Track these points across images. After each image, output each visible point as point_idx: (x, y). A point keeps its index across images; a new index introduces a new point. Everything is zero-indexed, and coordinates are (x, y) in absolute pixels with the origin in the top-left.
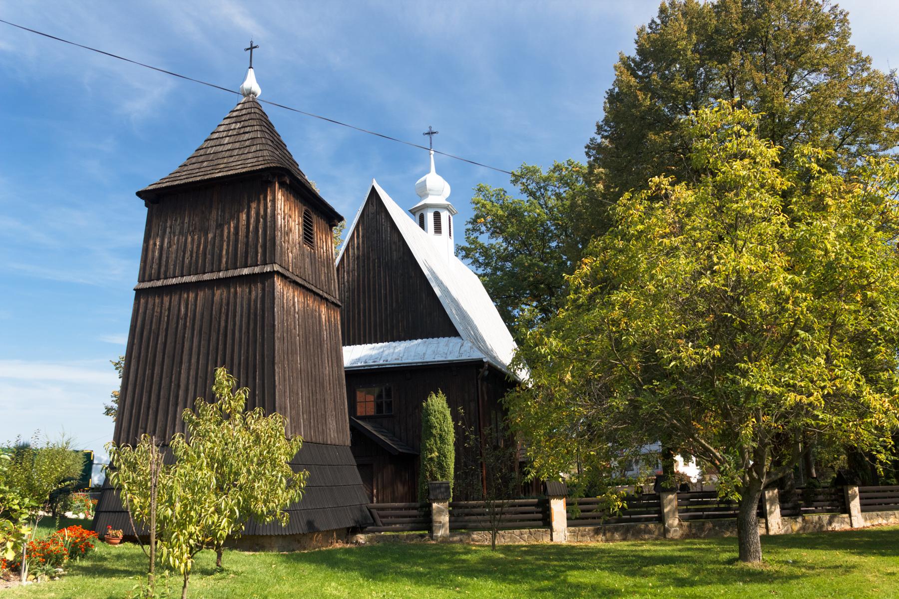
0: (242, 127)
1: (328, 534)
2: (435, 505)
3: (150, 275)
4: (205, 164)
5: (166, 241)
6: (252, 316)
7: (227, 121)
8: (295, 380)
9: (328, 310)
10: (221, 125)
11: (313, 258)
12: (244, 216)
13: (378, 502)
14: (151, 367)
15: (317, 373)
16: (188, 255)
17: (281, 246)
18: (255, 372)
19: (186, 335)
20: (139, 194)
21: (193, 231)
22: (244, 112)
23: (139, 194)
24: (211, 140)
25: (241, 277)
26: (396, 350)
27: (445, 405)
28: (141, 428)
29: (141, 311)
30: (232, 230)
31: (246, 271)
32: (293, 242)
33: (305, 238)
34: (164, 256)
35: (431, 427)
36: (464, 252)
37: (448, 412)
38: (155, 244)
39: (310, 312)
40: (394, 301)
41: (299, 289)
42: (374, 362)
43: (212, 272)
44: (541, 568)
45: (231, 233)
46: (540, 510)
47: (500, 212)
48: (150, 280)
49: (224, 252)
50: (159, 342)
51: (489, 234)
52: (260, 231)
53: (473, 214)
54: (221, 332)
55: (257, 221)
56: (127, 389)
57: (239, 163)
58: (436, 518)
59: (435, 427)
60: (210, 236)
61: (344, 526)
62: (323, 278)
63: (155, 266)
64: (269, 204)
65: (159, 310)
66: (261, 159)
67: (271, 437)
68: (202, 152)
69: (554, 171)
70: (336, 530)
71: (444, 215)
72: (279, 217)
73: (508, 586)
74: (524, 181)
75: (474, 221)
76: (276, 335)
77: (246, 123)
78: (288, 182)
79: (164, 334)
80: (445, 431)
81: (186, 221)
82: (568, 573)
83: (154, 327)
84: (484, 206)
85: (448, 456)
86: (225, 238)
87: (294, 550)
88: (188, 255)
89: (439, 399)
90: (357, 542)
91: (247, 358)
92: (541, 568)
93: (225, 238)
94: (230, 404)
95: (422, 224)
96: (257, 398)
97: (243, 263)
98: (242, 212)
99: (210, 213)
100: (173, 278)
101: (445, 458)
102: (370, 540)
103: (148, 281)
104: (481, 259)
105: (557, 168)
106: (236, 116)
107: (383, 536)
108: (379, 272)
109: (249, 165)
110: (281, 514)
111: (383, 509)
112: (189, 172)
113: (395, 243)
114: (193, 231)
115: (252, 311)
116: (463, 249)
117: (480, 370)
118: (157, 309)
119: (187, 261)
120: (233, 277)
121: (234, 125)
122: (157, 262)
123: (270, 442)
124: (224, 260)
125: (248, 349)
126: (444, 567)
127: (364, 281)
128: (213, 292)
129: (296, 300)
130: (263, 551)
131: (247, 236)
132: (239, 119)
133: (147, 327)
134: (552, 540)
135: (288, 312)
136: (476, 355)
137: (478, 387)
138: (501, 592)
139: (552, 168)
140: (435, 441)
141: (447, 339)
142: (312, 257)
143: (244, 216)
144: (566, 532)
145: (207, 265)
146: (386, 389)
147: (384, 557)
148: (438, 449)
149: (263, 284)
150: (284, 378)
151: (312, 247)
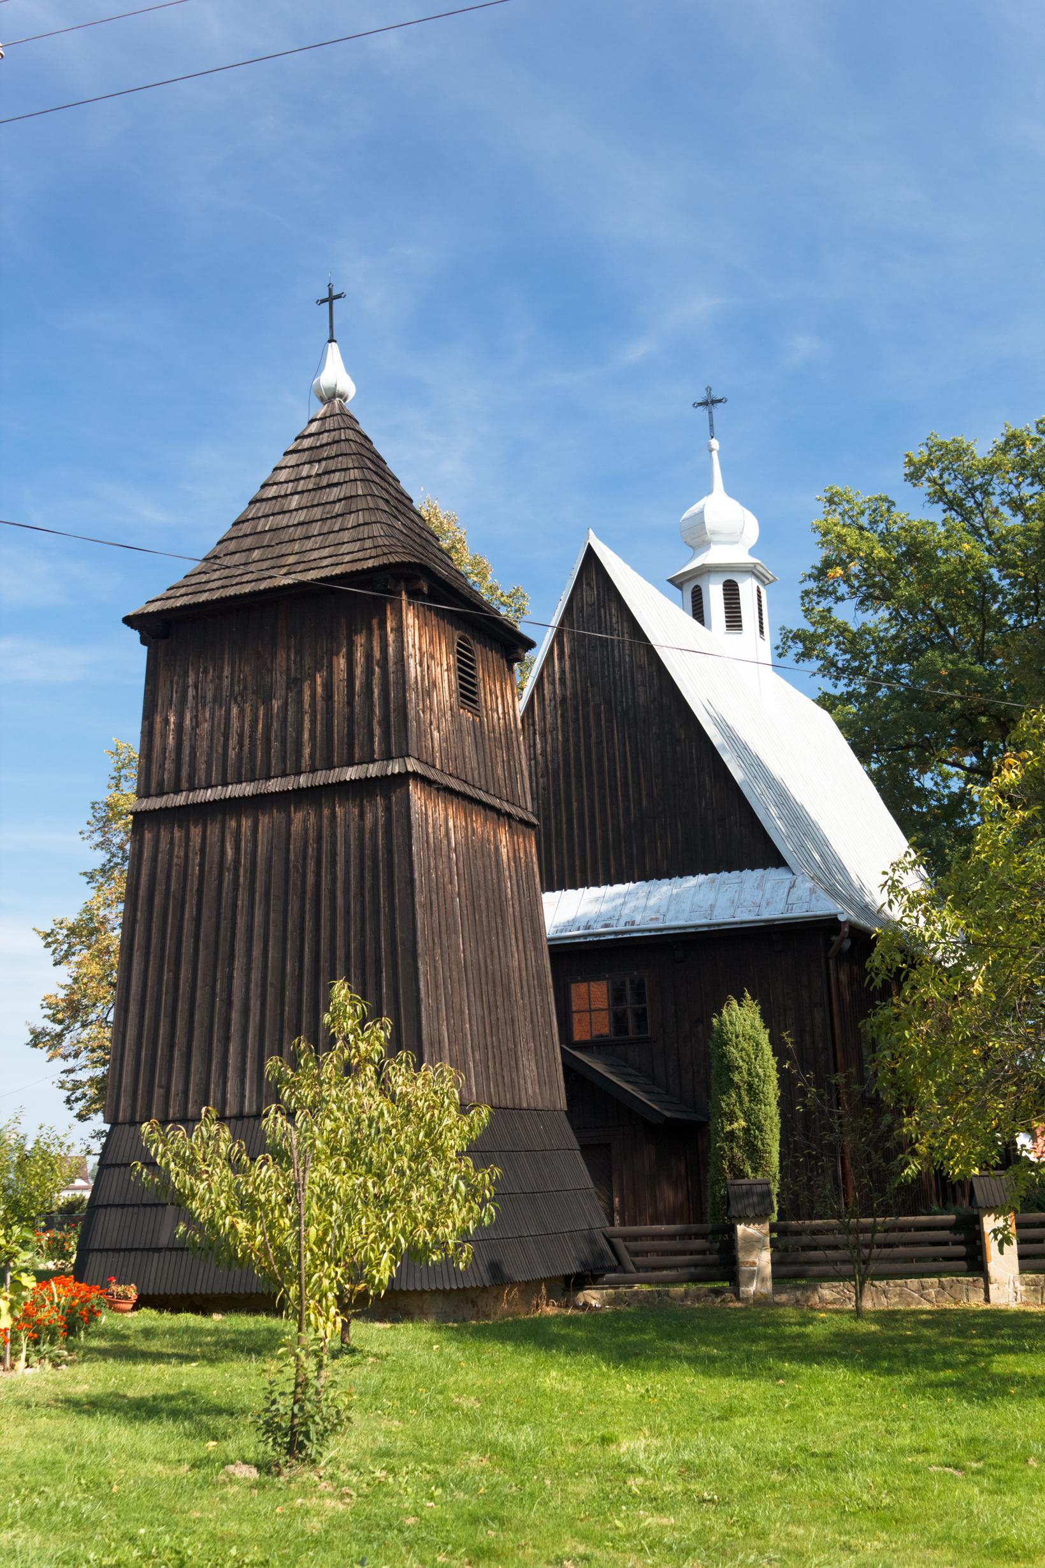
0: (324, 473)
1: (530, 1288)
2: (741, 1228)
3: (161, 783)
4: (256, 554)
5: (188, 716)
6: (368, 863)
7: (292, 460)
8: (456, 985)
9: (512, 836)
10: (281, 468)
11: (479, 733)
12: (342, 662)
13: (623, 1224)
15: (497, 967)
16: (233, 741)
17: (418, 722)
18: (378, 972)
19: (239, 903)
20: (129, 621)
22: (325, 439)
23: (129, 621)
24: (262, 500)
25: (341, 784)
26: (652, 901)
27: (759, 1023)
28: (160, 1086)
29: (145, 855)
30: (319, 690)
31: (351, 773)
32: (439, 709)
34: (186, 744)
35: (730, 1067)
36: (800, 645)
37: (764, 1037)
38: (166, 721)
39: (477, 846)
40: (644, 792)
41: (455, 800)
42: (606, 926)
43: (284, 774)
44: (945, 1349)
45: (319, 697)
46: (961, 1237)
47: (880, 552)
48: (161, 793)
49: (306, 736)
50: (186, 916)
51: (856, 600)
52: (376, 691)
53: (817, 557)
54: (309, 895)
56: (126, 1011)
57: (326, 552)
59: (738, 1068)
60: (276, 704)
61: (561, 1273)
62: (500, 771)
63: (169, 765)
64: (391, 638)
65: (182, 854)
66: (368, 543)
67: (434, 1107)
68: (247, 528)
69: (1004, 449)
70: (544, 1280)
71: (747, 588)
72: (412, 661)
73: (876, 1377)
74: (935, 474)
75: (820, 573)
76: (417, 899)
77: (332, 465)
78: (425, 589)
79: (194, 902)
80: (758, 1075)
82: (997, 1357)
83: (173, 886)
84: (841, 539)
85: (767, 1128)
86: (306, 706)
87: (464, 1320)
88: (233, 741)
89: (745, 1010)
90: (586, 1304)
91: (362, 947)
92: (945, 1349)
93: (306, 706)
94: (358, 1048)
95: (698, 612)
97: (345, 757)
98: (337, 654)
99: (274, 656)
100: (207, 788)
101: (761, 1131)
102: (614, 1301)
103: (157, 796)
104: (842, 660)
105: (1013, 441)
106: (311, 449)
107: (636, 1293)
109: (347, 558)
110: (457, 1246)
111: (635, 1238)
112: (226, 572)
113: (640, 667)
114: (241, 694)
115: (367, 852)
116: (798, 636)
117: (833, 938)
118: (178, 852)
119: (232, 754)
120: (327, 787)
121: (307, 467)
122: (173, 756)
123: (433, 1115)
124: (307, 751)
125: (363, 929)
126: (761, 1346)
127: (577, 752)
128: (289, 816)
129: (451, 824)
130: (412, 1320)
131: (350, 703)
132: (316, 455)
133: (160, 888)
134: (987, 1300)
135: (437, 850)
136: (825, 907)
137: (828, 975)
138: (860, 1386)
139: (1000, 440)
140: (739, 1096)
141: (759, 872)
142: (478, 734)
144: (1018, 1284)
145: (273, 762)
146: (632, 982)
147: (642, 1331)
148: (744, 1113)
149: (387, 798)
150: (436, 982)
151: (476, 712)
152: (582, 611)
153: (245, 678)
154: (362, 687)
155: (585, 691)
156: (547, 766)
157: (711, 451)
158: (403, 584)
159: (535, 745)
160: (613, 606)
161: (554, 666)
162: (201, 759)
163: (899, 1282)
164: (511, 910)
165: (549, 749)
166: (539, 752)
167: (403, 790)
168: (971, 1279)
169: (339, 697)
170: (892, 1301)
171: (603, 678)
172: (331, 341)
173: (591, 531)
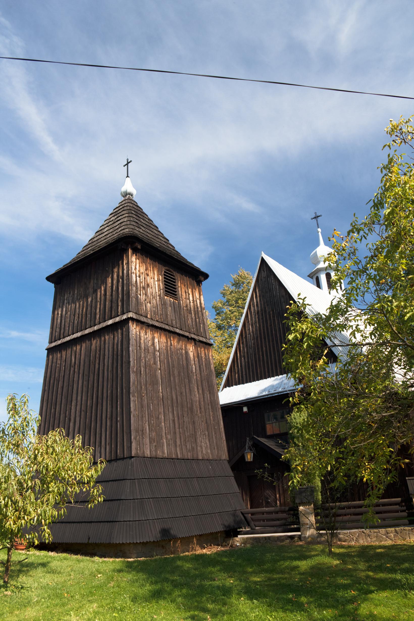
2: (301, 508)
6: (115, 357)
11: (177, 309)
12: (109, 280)
13: (251, 508)
14: (54, 407)
16: (76, 318)
18: (117, 402)
19: (75, 379)
21: (80, 299)
25: (108, 326)
33: (166, 291)
34: (63, 321)
38: (58, 314)
43: (91, 327)
49: (98, 310)
50: (59, 387)
55: (118, 281)
58: (303, 519)
60: (90, 300)
63: (58, 330)
64: (125, 267)
65: (60, 363)
79: (62, 381)
81: (76, 292)
86: (99, 299)
88: (76, 318)
93: (99, 299)
95: (318, 285)
96: (118, 424)
98: (108, 277)
108: (274, 320)
113: (283, 296)
115: (115, 353)
118: (59, 362)
119: (76, 322)
120: (103, 328)
124: (98, 316)
127: (264, 330)
128: (91, 342)
131: (112, 295)
133: (53, 377)
143: (109, 280)
152: (262, 280)
153: (81, 293)
154: (116, 288)
155: (265, 308)
156: (254, 336)
157: (318, 232)
158: (129, 246)
159: (249, 329)
160: (272, 276)
161: (254, 301)
162: (67, 325)
163: (376, 530)
164: (195, 377)
165: (254, 330)
166: (251, 331)
167: (128, 325)
168: (410, 528)
169: (108, 294)
170: (373, 540)
171: (270, 302)
172: (128, 176)
173: (262, 252)
